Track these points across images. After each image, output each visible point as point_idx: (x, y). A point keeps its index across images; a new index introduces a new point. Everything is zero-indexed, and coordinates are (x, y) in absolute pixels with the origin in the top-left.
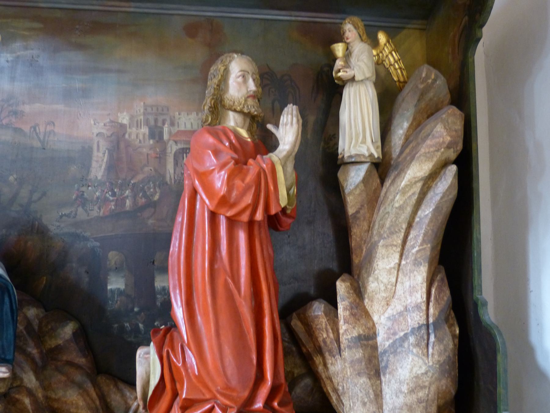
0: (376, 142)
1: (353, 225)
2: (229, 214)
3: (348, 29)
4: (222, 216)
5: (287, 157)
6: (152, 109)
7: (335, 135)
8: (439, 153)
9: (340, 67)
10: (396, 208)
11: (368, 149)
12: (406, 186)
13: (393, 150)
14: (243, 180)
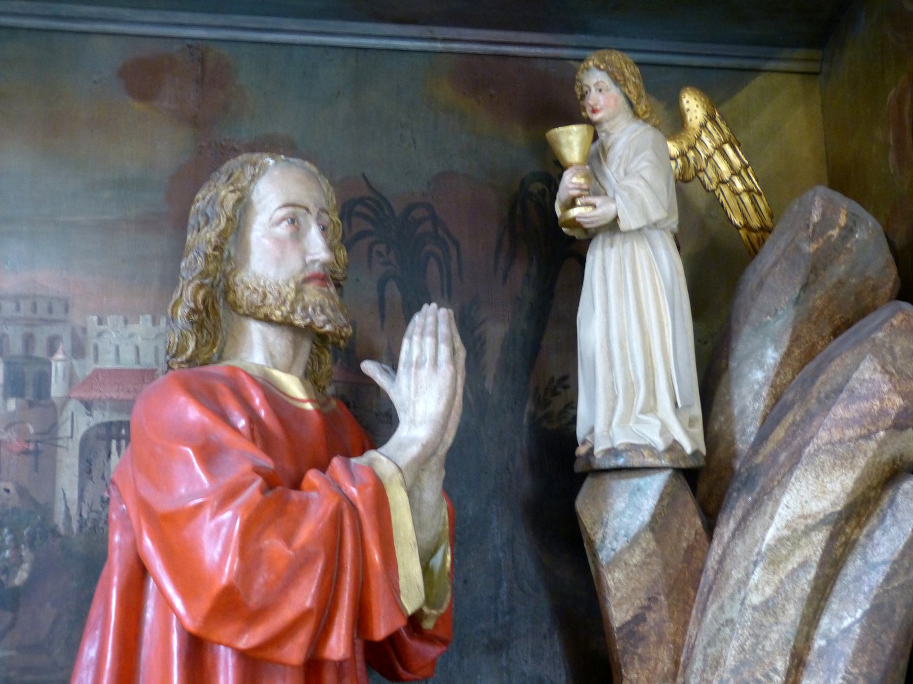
0: (688, 406)
1: (627, 658)
2: (245, 642)
3: (597, 84)
4: (222, 648)
5: (422, 462)
6: (18, 308)
7: (565, 378)
8: (873, 445)
9: (575, 192)
10: (755, 608)
11: (664, 431)
12: (780, 541)
13: (738, 428)
14: (288, 539)
